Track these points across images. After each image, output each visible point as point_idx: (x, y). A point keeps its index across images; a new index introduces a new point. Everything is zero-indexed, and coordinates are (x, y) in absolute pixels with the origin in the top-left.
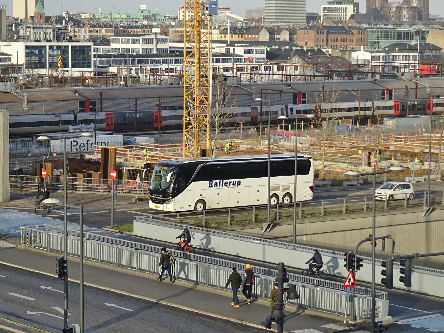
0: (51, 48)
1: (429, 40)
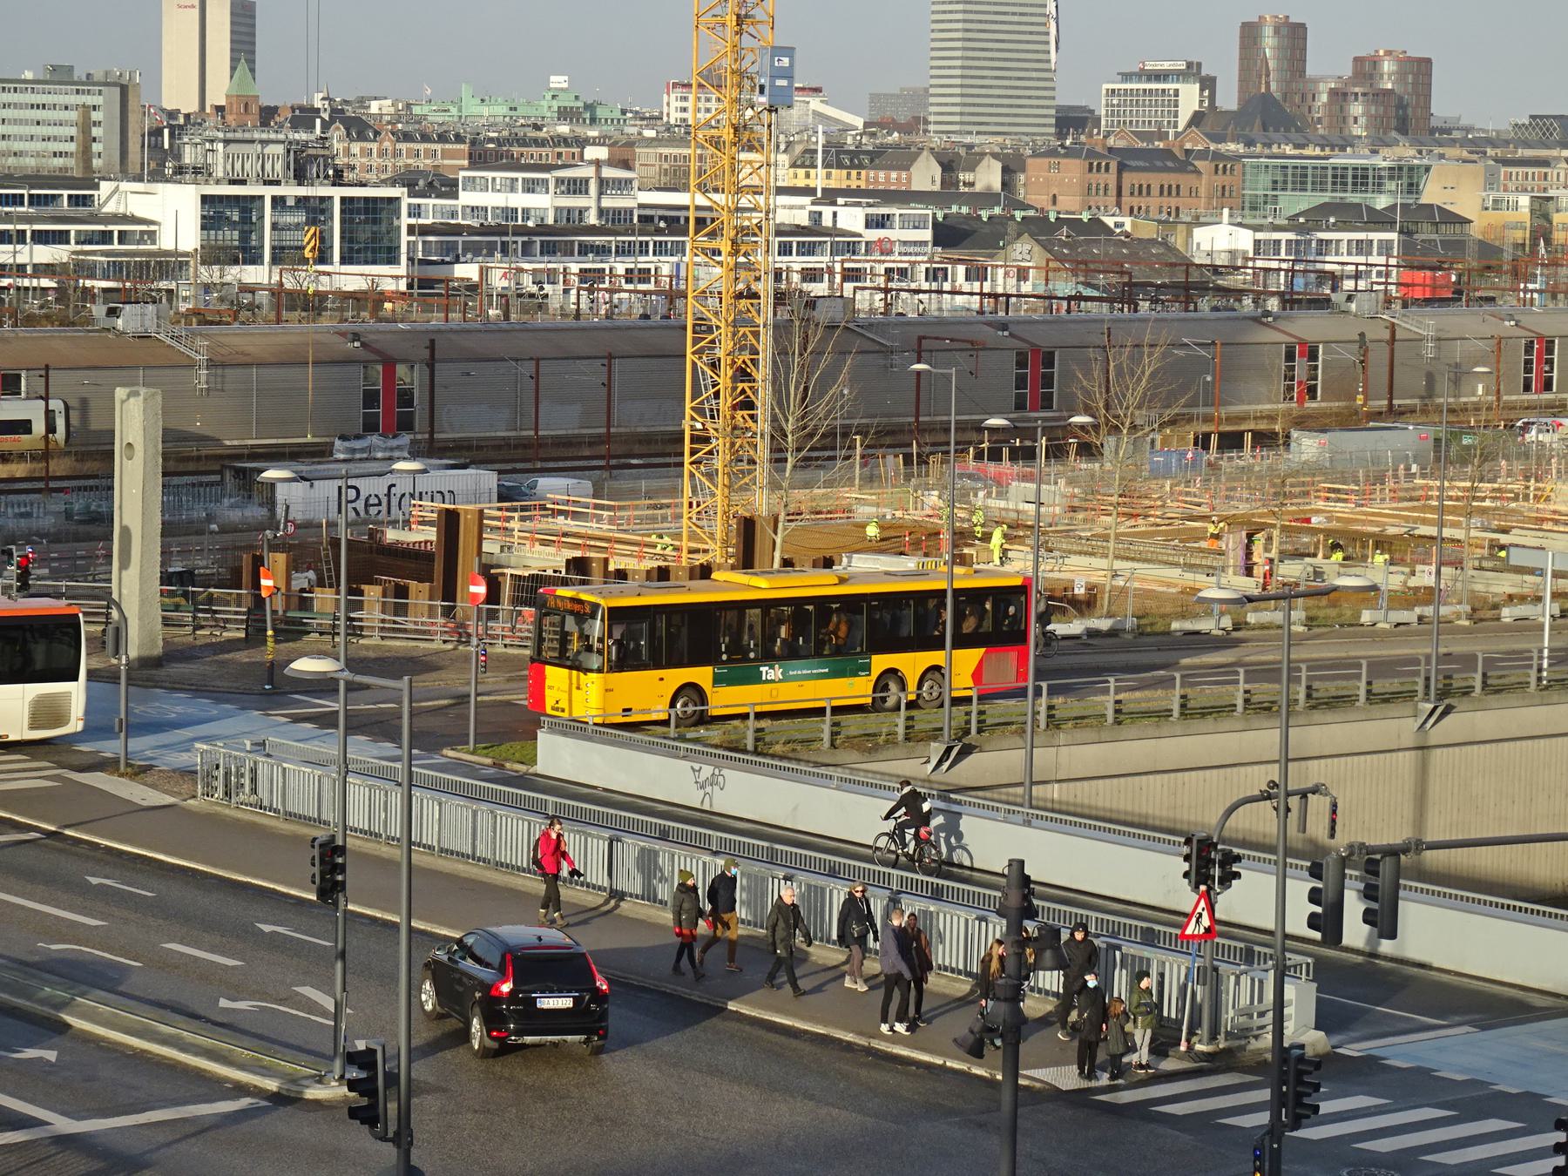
0: (278, 202)
1: (1432, 193)
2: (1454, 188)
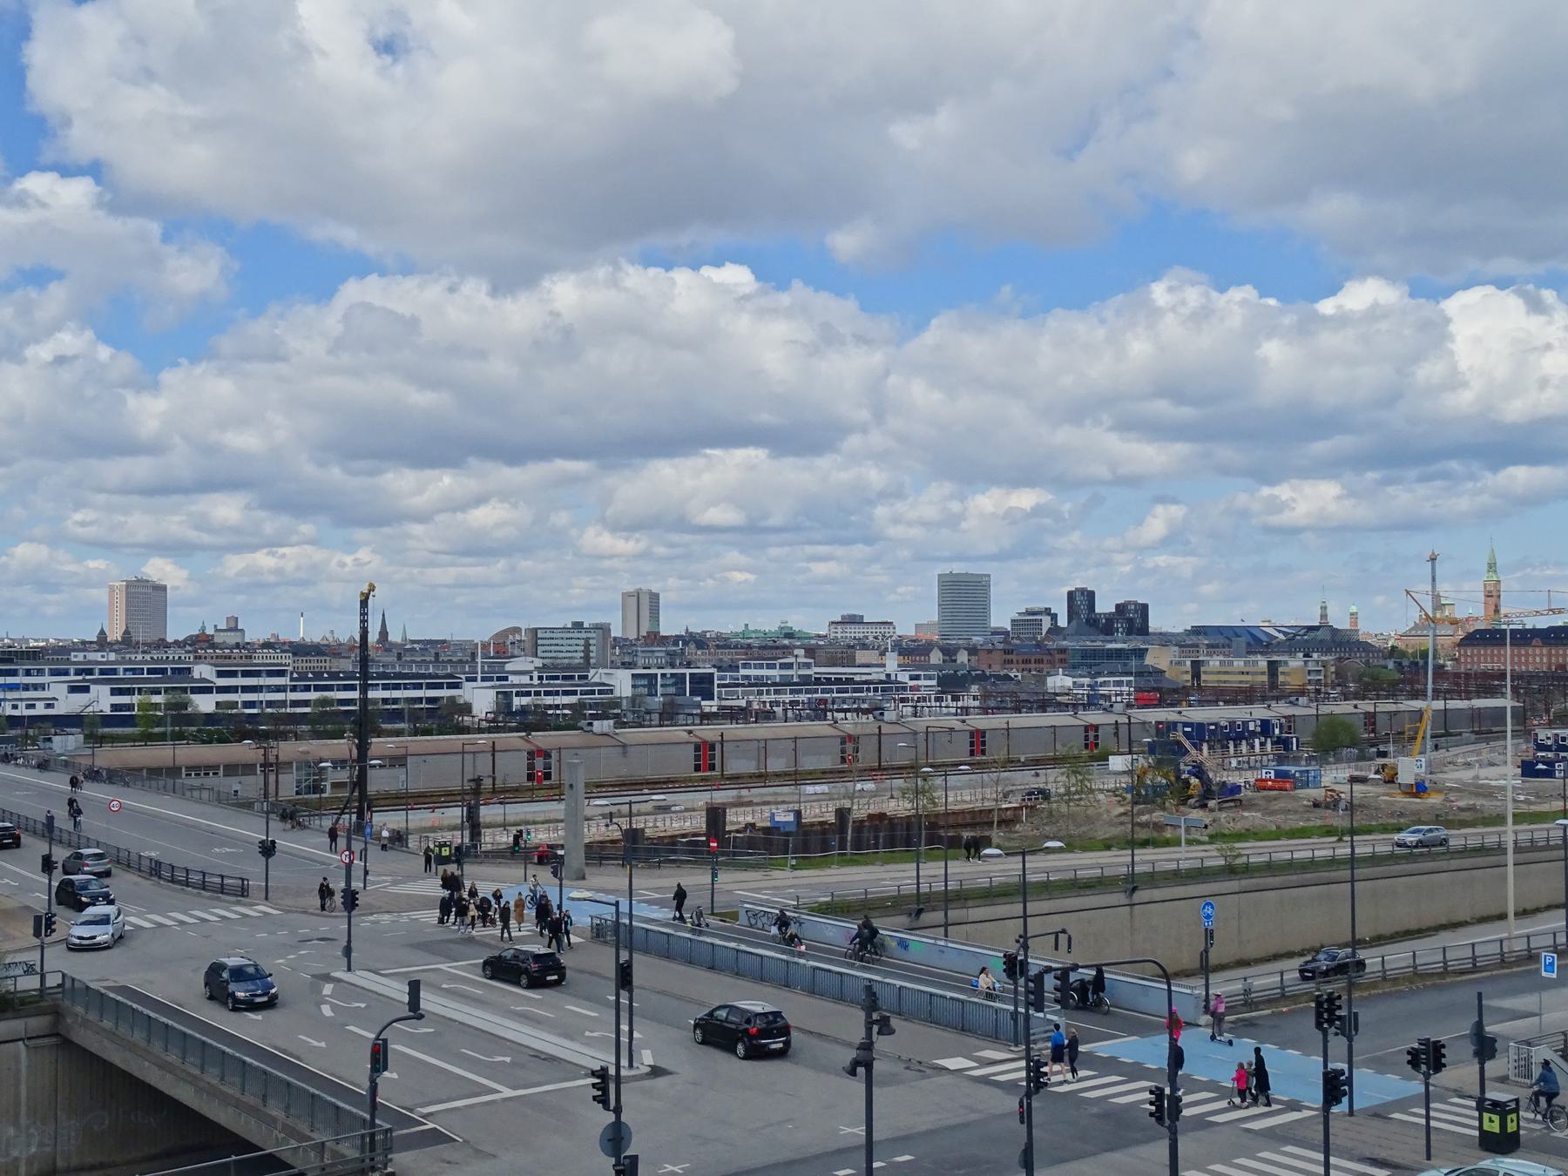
0: (663, 675)
1: (1149, 660)
2: (1158, 658)
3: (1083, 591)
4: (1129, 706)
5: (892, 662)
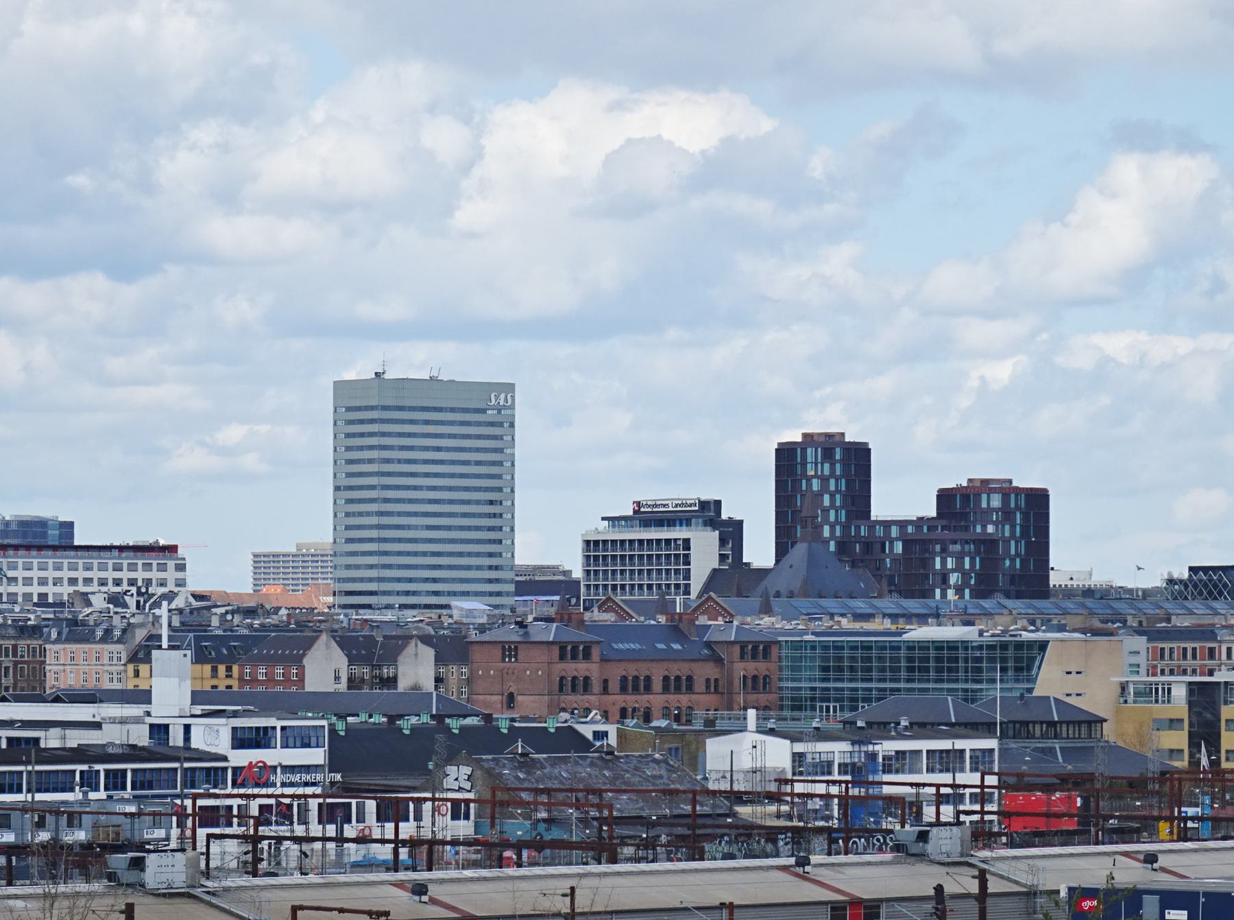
2: (1078, 675)
3: (829, 445)
4: (982, 836)
5: (172, 685)
